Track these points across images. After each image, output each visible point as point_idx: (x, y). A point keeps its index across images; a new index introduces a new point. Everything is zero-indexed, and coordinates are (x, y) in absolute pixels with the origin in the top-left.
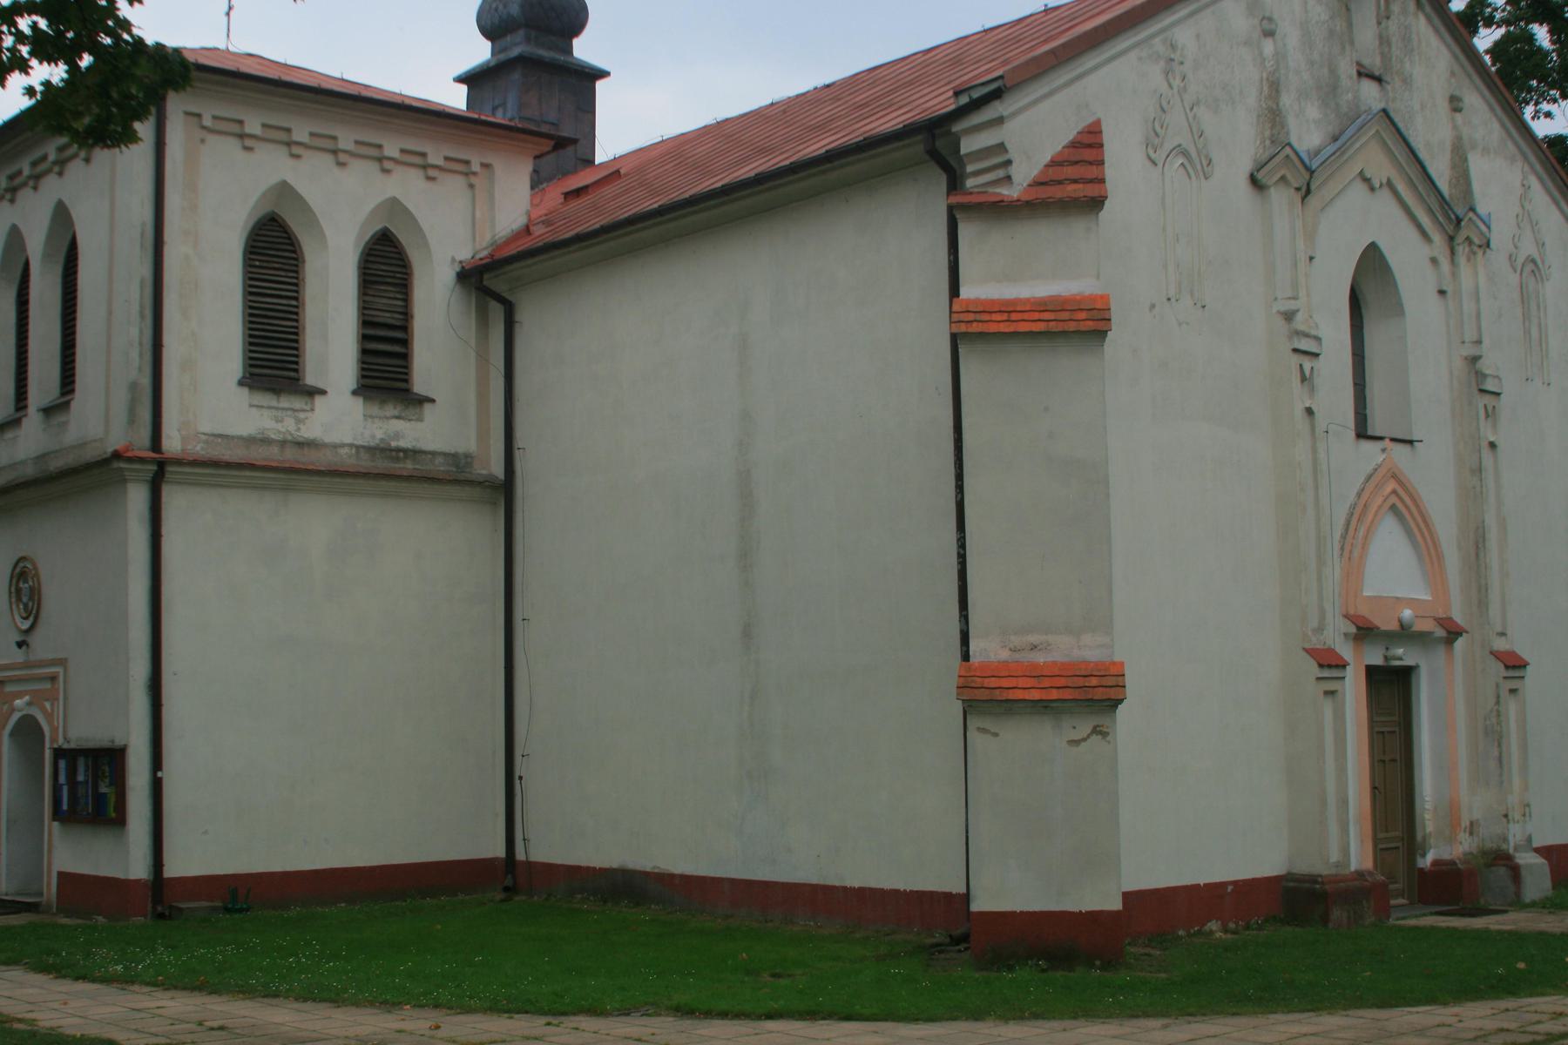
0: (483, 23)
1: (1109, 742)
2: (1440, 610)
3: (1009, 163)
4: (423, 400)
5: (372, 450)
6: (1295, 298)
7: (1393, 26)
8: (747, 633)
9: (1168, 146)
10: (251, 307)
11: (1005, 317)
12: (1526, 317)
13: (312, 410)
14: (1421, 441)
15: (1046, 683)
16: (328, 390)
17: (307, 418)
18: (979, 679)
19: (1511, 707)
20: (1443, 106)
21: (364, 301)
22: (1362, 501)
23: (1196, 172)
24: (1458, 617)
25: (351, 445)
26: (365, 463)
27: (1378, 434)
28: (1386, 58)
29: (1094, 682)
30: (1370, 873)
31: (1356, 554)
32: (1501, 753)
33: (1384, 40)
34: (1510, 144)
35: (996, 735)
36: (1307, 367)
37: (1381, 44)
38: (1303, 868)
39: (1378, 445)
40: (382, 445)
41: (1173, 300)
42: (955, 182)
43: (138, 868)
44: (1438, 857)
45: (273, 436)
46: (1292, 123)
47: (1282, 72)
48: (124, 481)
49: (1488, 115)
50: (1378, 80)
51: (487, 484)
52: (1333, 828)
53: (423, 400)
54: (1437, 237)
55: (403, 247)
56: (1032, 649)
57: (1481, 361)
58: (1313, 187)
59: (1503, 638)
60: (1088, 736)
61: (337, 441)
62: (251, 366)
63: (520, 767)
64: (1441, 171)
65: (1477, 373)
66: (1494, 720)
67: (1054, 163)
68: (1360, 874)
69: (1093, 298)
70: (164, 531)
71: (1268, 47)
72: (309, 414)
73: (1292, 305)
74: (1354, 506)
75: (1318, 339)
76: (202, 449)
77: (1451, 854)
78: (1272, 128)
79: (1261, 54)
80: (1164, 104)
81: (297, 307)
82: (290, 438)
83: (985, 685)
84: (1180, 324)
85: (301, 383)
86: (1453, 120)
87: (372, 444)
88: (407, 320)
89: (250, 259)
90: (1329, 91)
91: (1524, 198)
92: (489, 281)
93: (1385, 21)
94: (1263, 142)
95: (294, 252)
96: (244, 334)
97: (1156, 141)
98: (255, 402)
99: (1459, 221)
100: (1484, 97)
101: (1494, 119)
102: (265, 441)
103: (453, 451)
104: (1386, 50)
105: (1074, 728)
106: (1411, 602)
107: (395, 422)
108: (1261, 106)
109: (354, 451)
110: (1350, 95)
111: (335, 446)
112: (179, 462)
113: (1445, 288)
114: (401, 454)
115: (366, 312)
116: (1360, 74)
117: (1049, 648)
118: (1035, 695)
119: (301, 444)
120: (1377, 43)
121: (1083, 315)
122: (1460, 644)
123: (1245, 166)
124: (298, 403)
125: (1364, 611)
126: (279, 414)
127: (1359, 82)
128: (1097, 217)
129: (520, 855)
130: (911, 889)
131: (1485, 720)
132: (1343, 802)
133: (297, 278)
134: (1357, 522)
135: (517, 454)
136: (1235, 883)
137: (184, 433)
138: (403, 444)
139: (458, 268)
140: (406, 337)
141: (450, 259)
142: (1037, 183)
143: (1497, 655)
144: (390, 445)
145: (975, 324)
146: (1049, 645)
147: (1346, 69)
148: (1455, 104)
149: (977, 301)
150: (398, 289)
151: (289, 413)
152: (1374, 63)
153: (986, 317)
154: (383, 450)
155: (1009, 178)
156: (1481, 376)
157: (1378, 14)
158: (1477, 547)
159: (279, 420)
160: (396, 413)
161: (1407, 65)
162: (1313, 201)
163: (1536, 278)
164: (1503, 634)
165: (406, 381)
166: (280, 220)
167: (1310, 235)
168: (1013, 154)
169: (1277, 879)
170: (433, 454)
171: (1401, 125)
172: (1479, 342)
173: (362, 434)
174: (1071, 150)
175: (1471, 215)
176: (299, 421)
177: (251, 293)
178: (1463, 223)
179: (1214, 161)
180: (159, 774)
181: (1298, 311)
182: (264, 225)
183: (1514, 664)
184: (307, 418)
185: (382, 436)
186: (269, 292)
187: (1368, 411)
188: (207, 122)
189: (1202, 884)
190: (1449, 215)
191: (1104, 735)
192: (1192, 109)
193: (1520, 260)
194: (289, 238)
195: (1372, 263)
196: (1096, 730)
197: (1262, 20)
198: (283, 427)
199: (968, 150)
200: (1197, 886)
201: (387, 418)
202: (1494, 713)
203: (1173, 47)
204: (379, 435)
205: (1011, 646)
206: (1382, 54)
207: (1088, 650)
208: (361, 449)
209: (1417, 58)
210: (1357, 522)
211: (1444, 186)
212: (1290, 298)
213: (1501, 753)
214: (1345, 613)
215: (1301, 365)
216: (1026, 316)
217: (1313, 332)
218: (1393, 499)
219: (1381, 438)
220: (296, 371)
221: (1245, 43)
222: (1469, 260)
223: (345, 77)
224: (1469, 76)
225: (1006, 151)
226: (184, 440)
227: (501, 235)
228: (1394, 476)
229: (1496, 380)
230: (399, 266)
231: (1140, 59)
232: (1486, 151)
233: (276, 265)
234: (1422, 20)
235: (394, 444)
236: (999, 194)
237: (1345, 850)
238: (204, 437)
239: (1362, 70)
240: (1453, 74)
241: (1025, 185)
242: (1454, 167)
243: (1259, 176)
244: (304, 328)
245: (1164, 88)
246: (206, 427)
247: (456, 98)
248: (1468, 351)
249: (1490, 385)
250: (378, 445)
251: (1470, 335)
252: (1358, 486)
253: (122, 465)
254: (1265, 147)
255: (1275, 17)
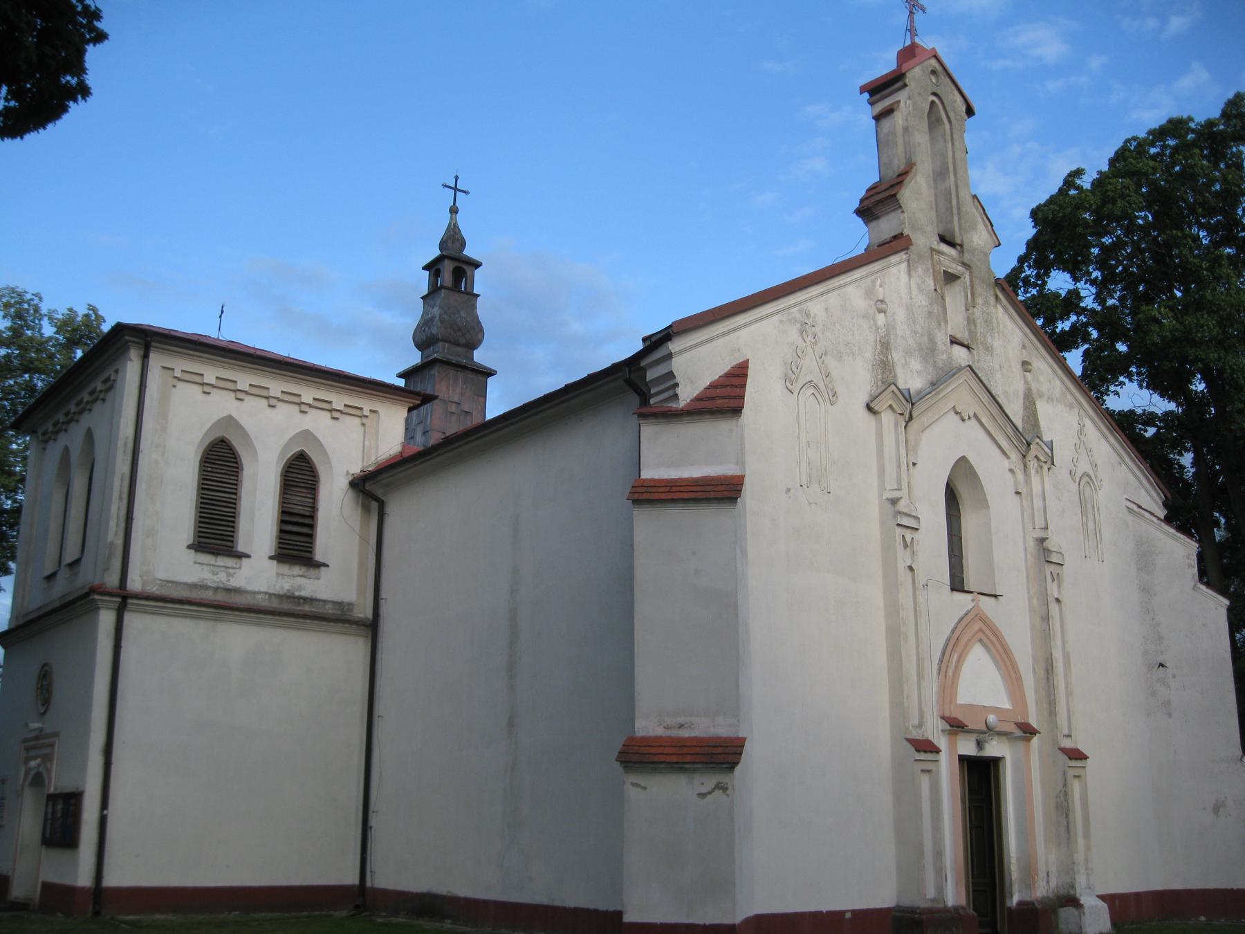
0: (416, 339)
1: (728, 795)
2: (1019, 717)
3: (677, 385)
4: (319, 565)
5: (280, 597)
6: (899, 489)
7: (977, 312)
8: (511, 723)
9: (802, 381)
10: (202, 498)
11: (668, 489)
12: (1084, 513)
13: (240, 568)
14: (1002, 596)
15: (685, 750)
16: (252, 555)
17: (235, 573)
18: (637, 748)
19: (1076, 787)
20: (1017, 368)
21: (283, 498)
22: (956, 636)
23: (824, 400)
24: (1034, 723)
25: (266, 593)
26: (275, 604)
27: (971, 590)
28: (972, 334)
29: (720, 750)
30: (963, 908)
31: (950, 673)
32: (1068, 823)
33: (971, 321)
34: (1069, 396)
35: (645, 788)
36: (908, 536)
37: (968, 323)
38: (907, 902)
39: (970, 596)
40: (289, 594)
41: (805, 487)
42: (644, 398)
43: (84, 878)
44: (1021, 899)
45: (210, 584)
46: (900, 372)
47: (892, 337)
48: (97, 609)
49: (1051, 375)
50: (968, 347)
51: (358, 623)
52: (930, 874)
53: (319, 565)
54: (1014, 456)
55: (314, 464)
56: (680, 727)
57: (1047, 541)
58: (914, 415)
59: (1069, 738)
60: (713, 790)
61: (257, 590)
62: (199, 537)
63: (374, 821)
64: (1016, 411)
65: (1044, 549)
66: (1062, 798)
67: (712, 386)
68: (956, 909)
69: (733, 477)
70: (124, 643)
71: (881, 319)
72: (237, 570)
73: (896, 494)
74: (948, 640)
75: (917, 518)
76: (157, 589)
77: (1031, 897)
78: (882, 373)
79: (875, 324)
80: (800, 354)
81: (236, 499)
82: (221, 586)
83: (640, 752)
84: (810, 504)
85: (234, 549)
86: (1024, 376)
87: (281, 593)
88: (314, 512)
89: (204, 466)
90: (929, 352)
91: (1080, 432)
92: (368, 486)
93: (972, 308)
94: (876, 382)
95: (236, 463)
96: (196, 515)
97: (793, 377)
98: (199, 561)
99: (1029, 444)
100: (1048, 363)
101: (1056, 379)
102: (204, 587)
103: (340, 601)
104: (973, 328)
105: (702, 784)
106: (995, 710)
107: (299, 579)
108: (875, 359)
109: (267, 597)
110: (945, 356)
111: (254, 593)
112: (137, 596)
113: (1019, 491)
114: (302, 601)
115: (285, 505)
116: (952, 342)
117: (692, 726)
118: (674, 759)
119: (228, 590)
120: (966, 323)
121: (723, 488)
122: (1035, 740)
123: (865, 398)
124: (230, 562)
125: (955, 715)
126: (216, 569)
127: (951, 348)
128: (737, 422)
129: (369, 884)
130: (661, 921)
131: (1056, 797)
132: (939, 854)
133: (237, 480)
134: (954, 649)
135: (382, 603)
136: (853, 912)
137: (145, 578)
138: (303, 594)
139: (350, 478)
140: (312, 523)
141: (345, 472)
142: (698, 399)
143: (1064, 751)
144: (294, 593)
145: (645, 494)
146: (693, 725)
147: (942, 339)
148: (1025, 365)
149: (652, 480)
150: (309, 492)
151: (223, 569)
152: (962, 335)
153: (654, 490)
154: (289, 597)
155: (676, 396)
156: (1047, 551)
157: (966, 304)
158: (1048, 673)
159: (214, 573)
160: (301, 573)
161: (989, 340)
162: (914, 425)
163: (1091, 487)
164: (1069, 736)
165: (311, 552)
166: (227, 441)
167: (910, 446)
168: (679, 379)
169: (888, 910)
170: (325, 601)
171: (983, 379)
172: (1046, 528)
173: (275, 586)
174: (724, 378)
175: (1038, 440)
176: (229, 575)
177: (203, 489)
178: (1032, 446)
179: (839, 393)
180: (105, 812)
181: (901, 498)
182: (216, 444)
183: (1076, 755)
184: (235, 573)
185: (288, 588)
186: (216, 488)
187: (965, 576)
188: (178, 374)
189: (824, 912)
190: (1022, 441)
191: (725, 789)
192: (820, 358)
193: (1079, 475)
194: (233, 454)
195: (963, 467)
196: (719, 786)
197: (877, 302)
198: (218, 578)
199: (650, 379)
200: (821, 912)
201: (294, 576)
202: (1062, 793)
203: (808, 316)
204: (287, 587)
205: (665, 724)
206: (970, 330)
207: (720, 728)
208: (273, 596)
209: (996, 334)
210: (954, 649)
211: (1019, 422)
212: (896, 490)
213: (1068, 823)
214: (941, 715)
215: (903, 536)
216: (682, 489)
217: (913, 514)
218: (980, 635)
219: (971, 592)
220: (232, 541)
221: (864, 316)
222: (1037, 472)
223: (290, 356)
224: (1037, 349)
225: (675, 377)
226: (144, 583)
227: (382, 457)
228: (981, 619)
229: (1059, 555)
230: (310, 476)
231: (781, 321)
232: (1050, 399)
233: (223, 471)
234: (1000, 309)
235: (297, 594)
236: (671, 407)
237: (940, 890)
238: (159, 582)
239: (953, 340)
240: (1024, 347)
241: (688, 401)
242: (1025, 408)
243: (872, 405)
244: (239, 514)
245: (800, 342)
246: (161, 575)
247: (401, 383)
248: (1041, 534)
249: (1054, 558)
250: (285, 594)
251: (1039, 523)
252: (953, 625)
253: (97, 597)
254: (877, 386)
255: (887, 300)
